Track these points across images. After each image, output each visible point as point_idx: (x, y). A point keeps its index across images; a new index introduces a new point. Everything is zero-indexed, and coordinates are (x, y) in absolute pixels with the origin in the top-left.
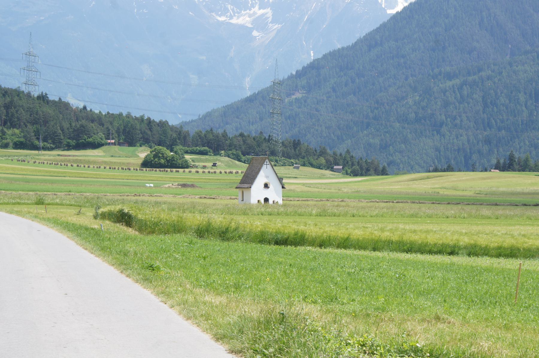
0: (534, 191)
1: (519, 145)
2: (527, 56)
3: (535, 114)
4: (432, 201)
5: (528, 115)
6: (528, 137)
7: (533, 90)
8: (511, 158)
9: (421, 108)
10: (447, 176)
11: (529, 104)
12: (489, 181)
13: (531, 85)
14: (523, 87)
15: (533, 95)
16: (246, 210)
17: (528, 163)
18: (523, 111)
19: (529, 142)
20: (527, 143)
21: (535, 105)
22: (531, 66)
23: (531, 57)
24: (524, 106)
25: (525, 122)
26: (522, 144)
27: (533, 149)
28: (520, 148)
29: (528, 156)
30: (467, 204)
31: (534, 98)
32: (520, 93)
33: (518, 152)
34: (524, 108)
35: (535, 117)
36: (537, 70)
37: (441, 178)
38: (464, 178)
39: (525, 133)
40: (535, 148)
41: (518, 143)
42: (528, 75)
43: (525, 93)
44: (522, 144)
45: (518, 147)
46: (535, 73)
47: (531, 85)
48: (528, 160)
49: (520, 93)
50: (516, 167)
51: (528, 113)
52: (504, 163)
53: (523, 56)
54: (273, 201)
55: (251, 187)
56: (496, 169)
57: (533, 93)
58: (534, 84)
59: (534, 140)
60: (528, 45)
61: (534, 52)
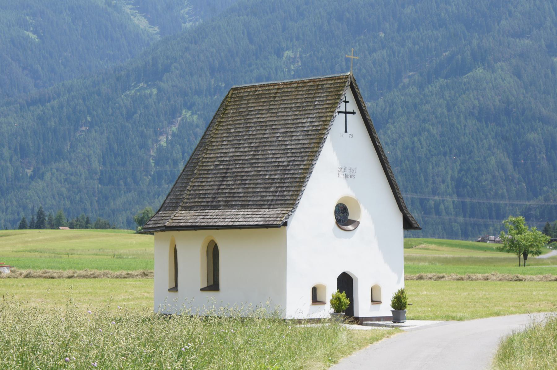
0: (463, 249)
1: (6, 205)
2: (9, 107)
3: (21, 171)
4: (418, 272)
5: (13, 172)
6: (15, 196)
7: (18, 144)
8: (40, 214)
9: (251, 68)
10: (16, 234)
11: (14, 159)
12: (77, 241)
13: (16, 138)
14: (7, 142)
15: (19, 150)
16: (25, 309)
17: (61, 221)
18: (7, 167)
19: (16, 202)
20: (15, 203)
21: (21, 161)
22: (14, 119)
23: (14, 109)
24: (8, 161)
25: (10, 179)
26: (9, 204)
27: (21, 209)
28: (7, 208)
29: (61, 214)
30: (458, 280)
31: (19, 153)
32: (4, 148)
33: (4, 213)
34: (9, 164)
35: (21, 175)
36: (21, 123)
37: (7, 237)
38: (41, 238)
39: (11, 192)
40: (24, 210)
41: (5, 203)
42: (12, 127)
43: (10, 148)
44: (9, 204)
45: (5, 207)
46: (19, 126)
47: (16, 138)
48: (61, 218)
49: (4, 148)
50: (46, 225)
51: (14, 170)
52: (44, 221)
53: (5, 107)
54: (314, 290)
55: (285, 224)
56: (22, 229)
57: (18, 147)
58: (19, 138)
59: (22, 199)
60: (7, 96)
61: (17, 104)
